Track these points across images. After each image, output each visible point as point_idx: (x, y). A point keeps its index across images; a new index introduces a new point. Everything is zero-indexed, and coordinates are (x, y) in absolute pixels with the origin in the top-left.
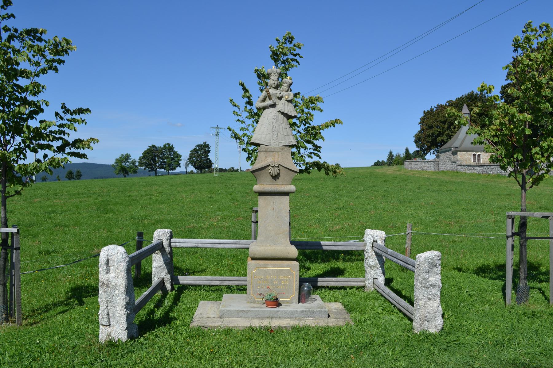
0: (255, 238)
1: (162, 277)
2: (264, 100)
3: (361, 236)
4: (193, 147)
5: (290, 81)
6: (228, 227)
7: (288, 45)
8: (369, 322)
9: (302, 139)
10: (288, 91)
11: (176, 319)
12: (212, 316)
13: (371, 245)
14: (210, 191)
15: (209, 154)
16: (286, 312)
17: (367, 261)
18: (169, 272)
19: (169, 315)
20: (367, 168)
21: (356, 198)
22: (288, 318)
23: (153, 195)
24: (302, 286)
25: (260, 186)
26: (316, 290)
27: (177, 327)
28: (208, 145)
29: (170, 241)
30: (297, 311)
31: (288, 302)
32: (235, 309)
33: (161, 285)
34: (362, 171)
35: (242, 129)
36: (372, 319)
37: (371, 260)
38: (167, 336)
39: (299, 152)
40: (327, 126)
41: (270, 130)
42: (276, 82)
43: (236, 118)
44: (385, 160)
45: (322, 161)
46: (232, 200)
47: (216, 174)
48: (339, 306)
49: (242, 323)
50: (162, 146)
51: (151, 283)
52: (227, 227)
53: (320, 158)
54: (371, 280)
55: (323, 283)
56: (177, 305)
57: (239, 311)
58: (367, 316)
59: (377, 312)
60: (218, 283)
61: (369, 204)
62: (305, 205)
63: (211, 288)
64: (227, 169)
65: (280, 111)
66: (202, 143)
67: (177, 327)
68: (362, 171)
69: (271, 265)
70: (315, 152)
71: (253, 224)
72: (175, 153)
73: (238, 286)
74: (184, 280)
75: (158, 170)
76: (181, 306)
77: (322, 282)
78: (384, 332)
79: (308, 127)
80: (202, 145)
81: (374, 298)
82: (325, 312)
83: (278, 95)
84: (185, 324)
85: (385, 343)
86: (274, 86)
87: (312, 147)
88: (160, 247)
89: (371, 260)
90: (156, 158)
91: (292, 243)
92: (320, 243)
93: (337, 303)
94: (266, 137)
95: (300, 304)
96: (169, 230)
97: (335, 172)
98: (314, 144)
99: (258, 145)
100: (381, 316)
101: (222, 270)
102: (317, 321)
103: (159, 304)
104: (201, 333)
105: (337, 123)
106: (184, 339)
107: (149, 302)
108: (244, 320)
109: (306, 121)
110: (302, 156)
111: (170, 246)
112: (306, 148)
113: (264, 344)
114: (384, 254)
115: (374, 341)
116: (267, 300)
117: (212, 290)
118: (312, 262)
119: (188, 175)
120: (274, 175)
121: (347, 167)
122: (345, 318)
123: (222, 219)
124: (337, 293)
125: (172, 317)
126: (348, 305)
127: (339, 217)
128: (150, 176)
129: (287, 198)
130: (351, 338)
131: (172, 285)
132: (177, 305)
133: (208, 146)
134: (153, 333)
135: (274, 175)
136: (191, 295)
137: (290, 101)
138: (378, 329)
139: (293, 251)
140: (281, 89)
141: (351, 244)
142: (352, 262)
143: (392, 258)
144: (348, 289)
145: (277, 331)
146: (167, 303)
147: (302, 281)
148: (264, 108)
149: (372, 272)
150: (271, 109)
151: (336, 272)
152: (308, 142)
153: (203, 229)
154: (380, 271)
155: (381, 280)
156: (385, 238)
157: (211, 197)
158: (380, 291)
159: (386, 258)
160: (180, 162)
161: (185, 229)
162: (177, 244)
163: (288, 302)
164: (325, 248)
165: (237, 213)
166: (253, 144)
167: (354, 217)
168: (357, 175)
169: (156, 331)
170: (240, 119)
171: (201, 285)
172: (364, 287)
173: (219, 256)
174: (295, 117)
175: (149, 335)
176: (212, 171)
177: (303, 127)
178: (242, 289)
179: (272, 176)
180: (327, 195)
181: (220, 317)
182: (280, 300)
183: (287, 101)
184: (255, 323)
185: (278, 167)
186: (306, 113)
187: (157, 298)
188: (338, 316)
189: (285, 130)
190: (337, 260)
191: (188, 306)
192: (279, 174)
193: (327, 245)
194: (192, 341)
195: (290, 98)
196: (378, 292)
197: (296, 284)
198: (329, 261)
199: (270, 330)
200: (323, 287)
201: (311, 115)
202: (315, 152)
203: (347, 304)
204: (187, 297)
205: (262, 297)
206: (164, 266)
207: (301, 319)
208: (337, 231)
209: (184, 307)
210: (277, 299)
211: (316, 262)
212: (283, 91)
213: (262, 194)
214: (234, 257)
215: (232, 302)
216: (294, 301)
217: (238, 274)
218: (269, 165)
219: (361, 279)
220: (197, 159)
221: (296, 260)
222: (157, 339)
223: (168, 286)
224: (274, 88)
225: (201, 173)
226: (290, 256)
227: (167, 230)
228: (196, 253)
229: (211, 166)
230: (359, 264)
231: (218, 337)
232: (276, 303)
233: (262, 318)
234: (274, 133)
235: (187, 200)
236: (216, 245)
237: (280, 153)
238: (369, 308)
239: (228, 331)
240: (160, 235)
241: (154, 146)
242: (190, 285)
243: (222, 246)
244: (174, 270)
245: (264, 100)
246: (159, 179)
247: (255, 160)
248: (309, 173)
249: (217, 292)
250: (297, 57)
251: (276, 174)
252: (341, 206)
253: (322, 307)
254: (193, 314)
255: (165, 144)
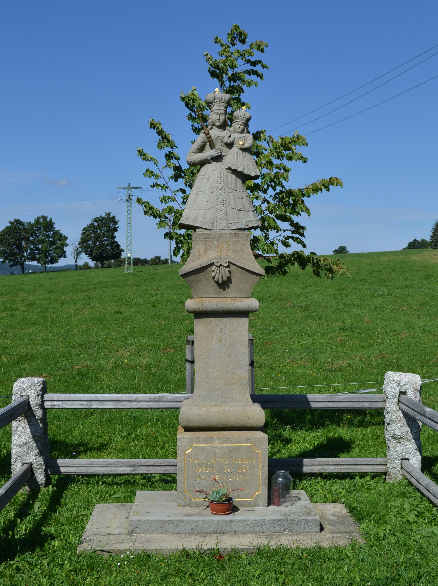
0: (192, 392)
1: (30, 461)
2: (201, 149)
3: (378, 383)
4: (88, 222)
5: (247, 115)
6: (148, 366)
7: (240, 47)
8: (393, 540)
9: (271, 213)
10: (242, 132)
11: (53, 538)
12: (117, 531)
13: (396, 400)
14: (118, 300)
15: (116, 234)
16: (245, 523)
17: (389, 428)
18: (41, 453)
19: (42, 531)
20: (395, 253)
21: (375, 309)
22: (250, 533)
23: (17, 309)
24: (274, 476)
25: (198, 300)
26: (301, 480)
27: (55, 552)
28: (114, 218)
29: (42, 398)
30: (264, 521)
31: (249, 504)
32: (156, 518)
33: (29, 472)
34: (386, 258)
35: (164, 200)
36: (398, 534)
37: (397, 426)
38: (36, 570)
39: (267, 237)
40: (316, 190)
41: (215, 201)
42: (222, 118)
43: (153, 181)
44: (428, 239)
45: (307, 252)
46: (156, 316)
47: (128, 270)
48: (339, 509)
49: (167, 543)
50: (33, 222)
51: (11, 473)
52: (146, 366)
53: (304, 246)
54: (398, 462)
55: (313, 468)
56: (55, 512)
57: (163, 523)
58: (389, 527)
59: (408, 521)
60: (127, 470)
61: (397, 320)
62: (283, 324)
63: (116, 480)
64: (149, 259)
65: (229, 169)
66: (104, 215)
67: (55, 552)
68: (386, 258)
69: (219, 439)
70: (296, 236)
71: (188, 365)
72: (57, 233)
73: (164, 474)
74: (67, 466)
75: (27, 263)
76: (63, 513)
77: (310, 465)
78: (418, 558)
79: (281, 192)
80: (103, 218)
81: (403, 495)
82: (314, 521)
83: (226, 140)
84: (69, 546)
85: (420, 578)
86: (218, 124)
87: (289, 227)
88: (24, 410)
89: (397, 426)
90: (23, 243)
91: (255, 399)
92: (307, 398)
93: (337, 504)
94: (205, 213)
95: (272, 507)
96: (40, 379)
97: (330, 270)
98: (292, 222)
99: (194, 228)
100: (414, 527)
101: (135, 446)
102: (299, 537)
103: (24, 511)
104: (96, 563)
105: (333, 184)
106: (67, 576)
107: (7, 508)
108: (173, 537)
109: (275, 181)
110: (272, 244)
111: (42, 406)
112: (278, 230)
113: (206, 581)
114: (418, 417)
115: (400, 575)
116: (213, 502)
117: (117, 484)
118: (294, 429)
119: (78, 272)
120: (220, 281)
121: (359, 251)
122: (350, 532)
123: (138, 352)
124: (337, 486)
125: (45, 535)
126: (355, 508)
127: (343, 345)
128: (12, 274)
129: (244, 322)
130: (360, 570)
131: (47, 475)
132: (55, 512)
133: (113, 220)
134: (12, 565)
135: (220, 281)
136: (81, 492)
137: (245, 150)
138: (407, 552)
139: (257, 414)
140: (232, 129)
141: (363, 399)
142: (366, 427)
143: (433, 423)
144: (357, 478)
145: (230, 557)
146: (38, 507)
147: (274, 465)
148: (202, 163)
149: (399, 447)
150: (214, 165)
151: (335, 448)
152: (283, 218)
153: (105, 370)
154: (412, 446)
155: (415, 461)
156: (421, 387)
157: (119, 312)
158: (413, 480)
159: (423, 422)
160: (65, 249)
161: (72, 371)
162: (55, 403)
163: (249, 504)
164: (314, 406)
165: (163, 341)
166: (182, 226)
167: (370, 345)
168: (376, 269)
169: (17, 562)
170: (160, 181)
171: (99, 475)
172: (385, 474)
173: (134, 419)
174: (256, 177)
175: (5, 568)
176: (121, 263)
177: (271, 192)
178: (168, 481)
179: (217, 282)
180: (323, 305)
181: (131, 533)
182: (236, 500)
183: (241, 149)
184: (192, 543)
185: (228, 266)
186: (277, 167)
187: (21, 499)
188: (339, 528)
189: (239, 202)
190: (338, 425)
191: (75, 512)
192: (229, 280)
193: (319, 400)
194: (79, 579)
195: (247, 145)
196: (410, 483)
197: (262, 471)
198: (323, 426)
199: (217, 555)
200: (313, 475)
201: (287, 171)
202: (296, 236)
203: (353, 505)
204: (73, 496)
205: (204, 495)
206: (32, 443)
207: (272, 535)
208: (340, 370)
209: (67, 514)
210: (229, 500)
211: (301, 428)
212: (235, 132)
213: (201, 314)
214: (157, 420)
215: (151, 504)
216: (260, 502)
217: (164, 451)
218: (212, 264)
219: (380, 459)
220: (95, 244)
221: (264, 429)
222: (18, 575)
223: (40, 478)
224: (219, 127)
225: (103, 267)
226: (252, 423)
227: (36, 380)
228: (92, 414)
229: (120, 254)
230: (377, 430)
231: (126, 569)
232: (228, 506)
233: (203, 534)
234: (220, 206)
235: (78, 317)
236: (123, 403)
237: (231, 243)
238: (392, 513)
239: (144, 559)
240: (26, 387)
241: (18, 222)
242: (78, 475)
243: (134, 405)
244: (51, 447)
245: (201, 149)
246: (29, 280)
247: (188, 253)
248: (285, 273)
249: (125, 486)
250: (258, 68)
251: (225, 279)
252: (348, 324)
253: (309, 513)
254: (83, 528)
255: (39, 218)
